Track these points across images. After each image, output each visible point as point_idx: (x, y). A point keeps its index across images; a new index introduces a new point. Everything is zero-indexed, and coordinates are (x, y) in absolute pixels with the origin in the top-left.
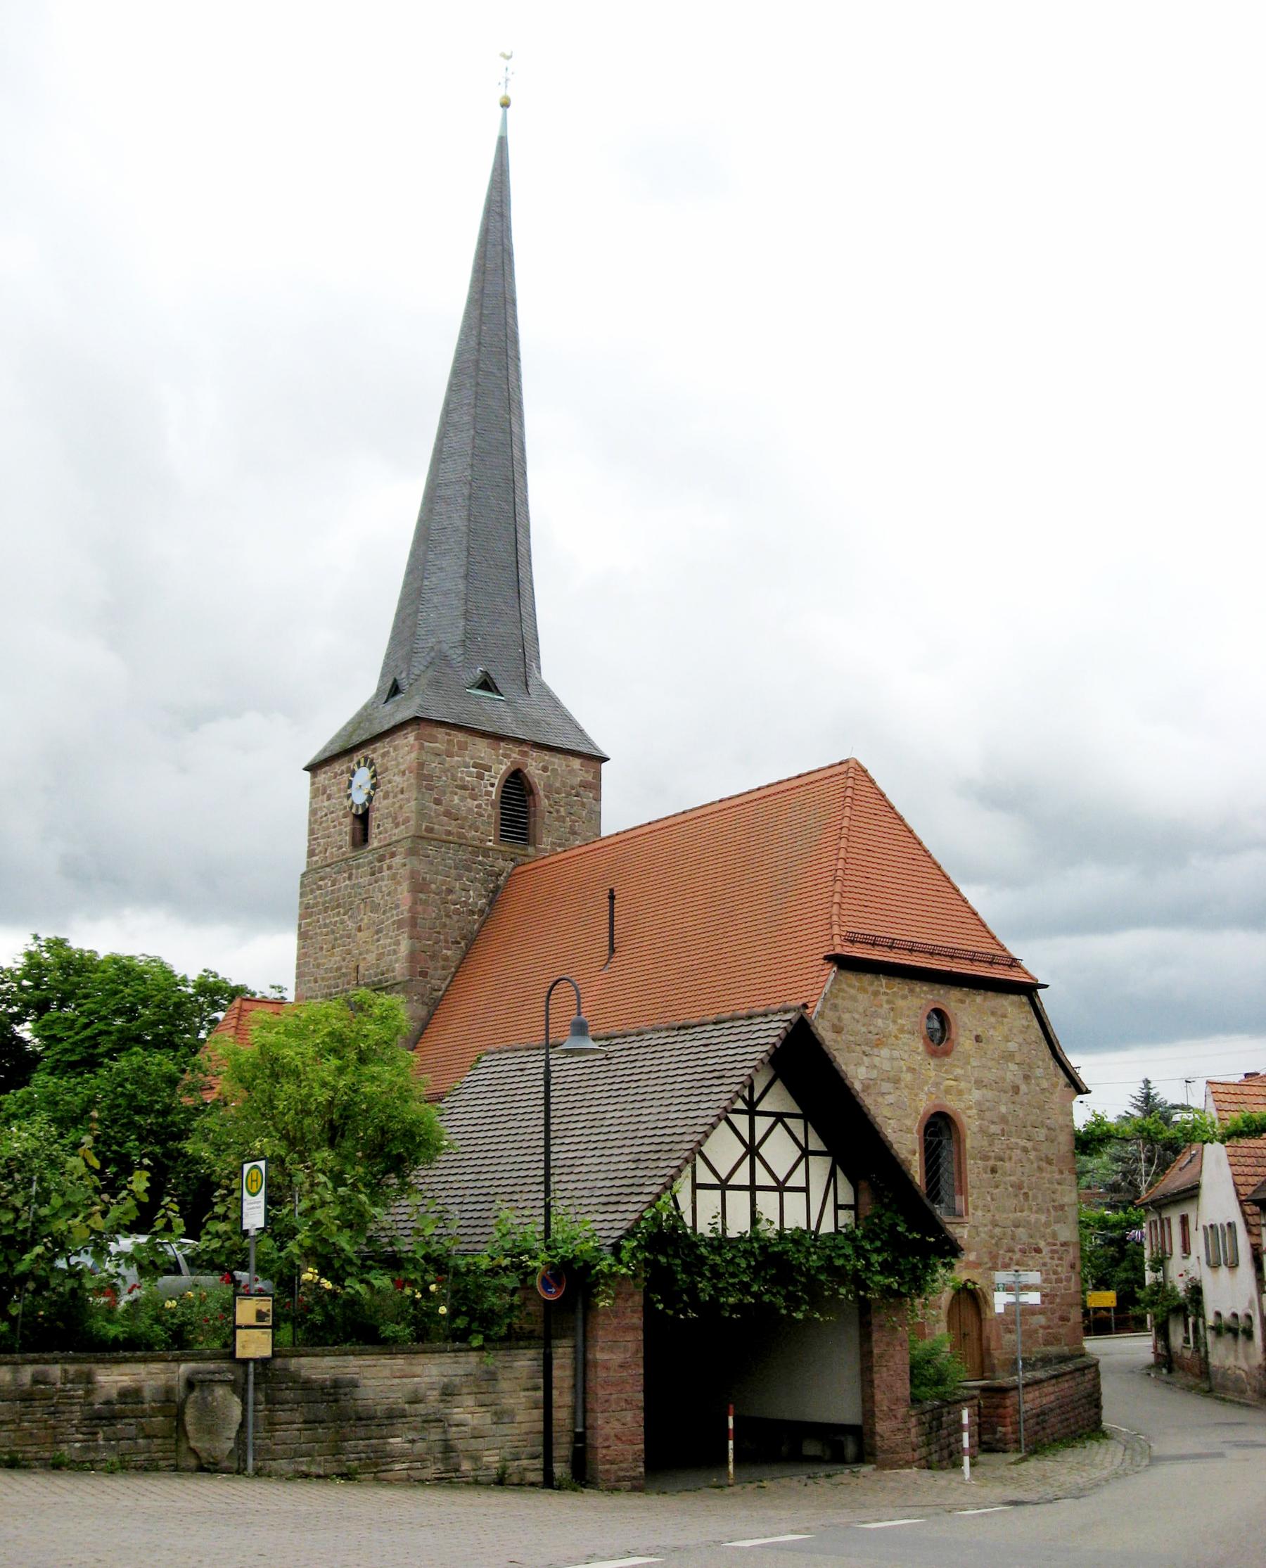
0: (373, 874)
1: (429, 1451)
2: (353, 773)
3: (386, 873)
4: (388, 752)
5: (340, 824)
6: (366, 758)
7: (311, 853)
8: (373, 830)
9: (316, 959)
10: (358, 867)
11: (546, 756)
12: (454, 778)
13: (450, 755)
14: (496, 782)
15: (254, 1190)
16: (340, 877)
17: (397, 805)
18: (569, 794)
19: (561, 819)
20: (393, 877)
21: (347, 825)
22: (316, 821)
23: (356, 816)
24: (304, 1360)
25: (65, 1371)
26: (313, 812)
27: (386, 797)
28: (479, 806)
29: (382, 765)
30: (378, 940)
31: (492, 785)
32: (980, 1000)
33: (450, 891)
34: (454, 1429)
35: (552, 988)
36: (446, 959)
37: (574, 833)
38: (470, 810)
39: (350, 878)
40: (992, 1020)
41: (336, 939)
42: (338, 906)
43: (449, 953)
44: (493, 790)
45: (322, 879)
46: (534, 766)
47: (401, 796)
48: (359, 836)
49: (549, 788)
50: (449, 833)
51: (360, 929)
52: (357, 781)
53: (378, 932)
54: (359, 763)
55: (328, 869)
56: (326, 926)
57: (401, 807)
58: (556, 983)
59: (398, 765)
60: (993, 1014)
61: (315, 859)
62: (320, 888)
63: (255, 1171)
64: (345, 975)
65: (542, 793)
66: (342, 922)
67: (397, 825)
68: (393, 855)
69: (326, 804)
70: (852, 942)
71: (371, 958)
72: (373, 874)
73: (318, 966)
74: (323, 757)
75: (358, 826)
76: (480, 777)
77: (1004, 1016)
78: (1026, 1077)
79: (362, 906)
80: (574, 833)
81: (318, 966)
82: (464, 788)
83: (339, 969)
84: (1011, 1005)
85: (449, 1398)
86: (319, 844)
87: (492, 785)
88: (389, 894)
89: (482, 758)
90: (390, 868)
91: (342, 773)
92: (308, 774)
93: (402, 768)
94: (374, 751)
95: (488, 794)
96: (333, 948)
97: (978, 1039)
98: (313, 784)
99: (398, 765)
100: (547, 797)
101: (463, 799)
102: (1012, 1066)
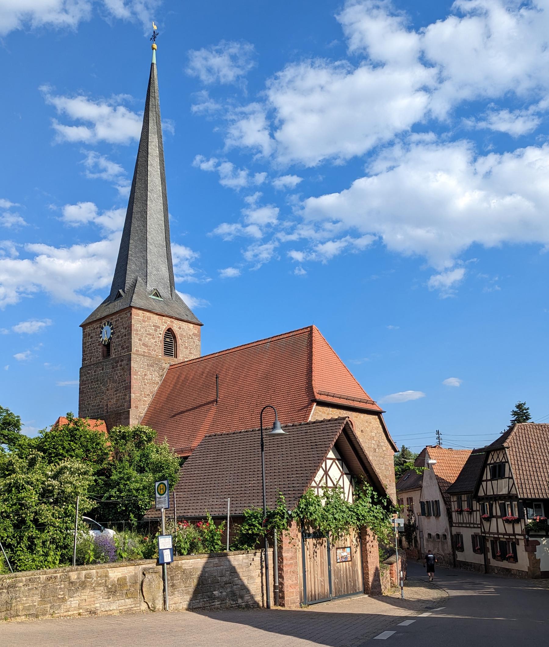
0: (113, 368)
1: (227, 595)
2: (102, 328)
3: (119, 368)
4: (118, 320)
5: (97, 348)
6: (108, 322)
7: (84, 360)
8: (112, 351)
9: (88, 402)
10: (106, 365)
11: (181, 323)
12: (146, 331)
13: (144, 321)
14: (162, 332)
15: (162, 493)
16: (98, 369)
17: (123, 341)
18: (189, 338)
19: (186, 348)
20: (123, 369)
21: (100, 349)
22: (86, 347)
23: (104, 345)
24: (183, 561)
25: (97, 572)
26: (84, 343)
27: (118, 337)
28: (156, 342)
29: (115, 325)
30: (116, 394)
31: (160, 334)
32: (363, 416)
33: (145, 375)
34: (235, 586)
35: (263, 411)
36: (144, 401)
37: (191, 353)
38: (152, 343)
39: (103, 370)
40: (367, 424)
41: (97, 394)
42: (98, 381)
43: (146, 399)
44: (161, 336)
45: (89, 370)
46: (176, 326)
47: (124, 337)
48: (105, 354)
49: (181, 335)
50: (144, 352)
51: (108, 390)
52: (104, 331)
53: (116, 391)
54: (105, 324)
55: (92, 366)
56: (92, 388)
57: (125, 342)
58: (264, 408)
59: (123, 325)
60: (367, 422)
61: (85, 362)
62: (88, 373)
63: (162, 485)
64: (101, 408)
65: (179, 338)
66: (99, 387)
67: (123, 349)
68: (122, 361)
69: (90, 340)
70: (321, 394)
71: (114, 401)
72: (113, 368)
73: (89, 404)
74: (88, 322)
75: (105, 349)
76: (156, 330)
77: (371, 423)
78: (378, 446)
79: (108, 381)
80: (191, 353)
81: (89, 404)
82: (150, 335)
83: (99, 405)
84: (373, 419)
85: (233, 574)
86: (88, 356)
87: (160, 334)
88: (121, 376)
89: (157, 323)
90: (121, 365)
91: (97, 328)
92: (82, 328)
93: (125, 326)
94: (112, 319)
95: (159, 337)
96: (96, 397)
97: (362, 431)
98: (84, 332)
99: (123, 325)
100: (181, 340)
101: (149, 339)
102: (374, 442)
